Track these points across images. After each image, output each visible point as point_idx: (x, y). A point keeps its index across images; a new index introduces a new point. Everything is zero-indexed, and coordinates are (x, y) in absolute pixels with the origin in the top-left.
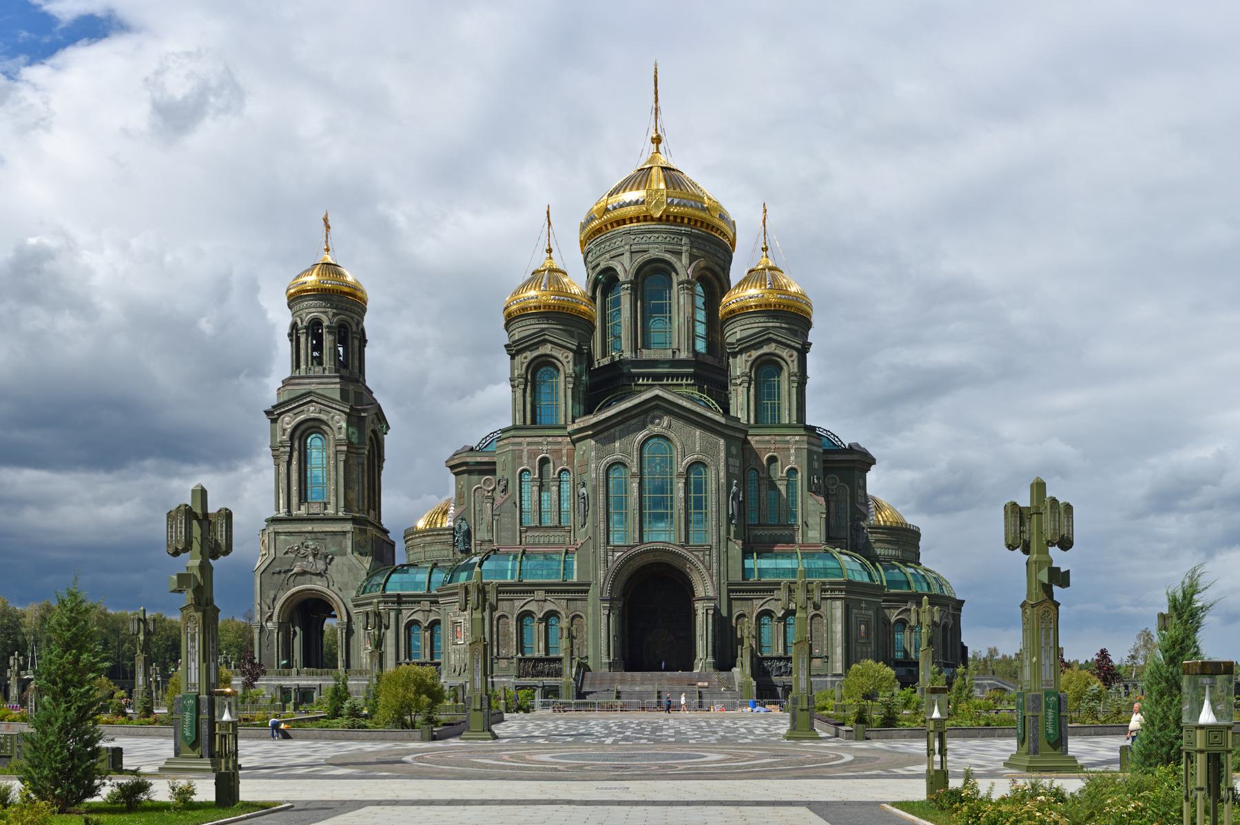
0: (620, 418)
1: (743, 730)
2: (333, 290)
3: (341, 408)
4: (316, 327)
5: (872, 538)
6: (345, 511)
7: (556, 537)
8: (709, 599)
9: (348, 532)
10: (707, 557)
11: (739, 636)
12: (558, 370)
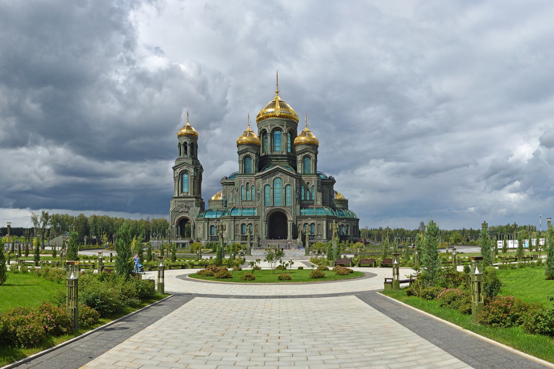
5: (335, 203)
7: (251, 203)
8: (291, 221)
9: (194, 201)
10: (291, 209)
11: (299, 231)
12: (251, 158)
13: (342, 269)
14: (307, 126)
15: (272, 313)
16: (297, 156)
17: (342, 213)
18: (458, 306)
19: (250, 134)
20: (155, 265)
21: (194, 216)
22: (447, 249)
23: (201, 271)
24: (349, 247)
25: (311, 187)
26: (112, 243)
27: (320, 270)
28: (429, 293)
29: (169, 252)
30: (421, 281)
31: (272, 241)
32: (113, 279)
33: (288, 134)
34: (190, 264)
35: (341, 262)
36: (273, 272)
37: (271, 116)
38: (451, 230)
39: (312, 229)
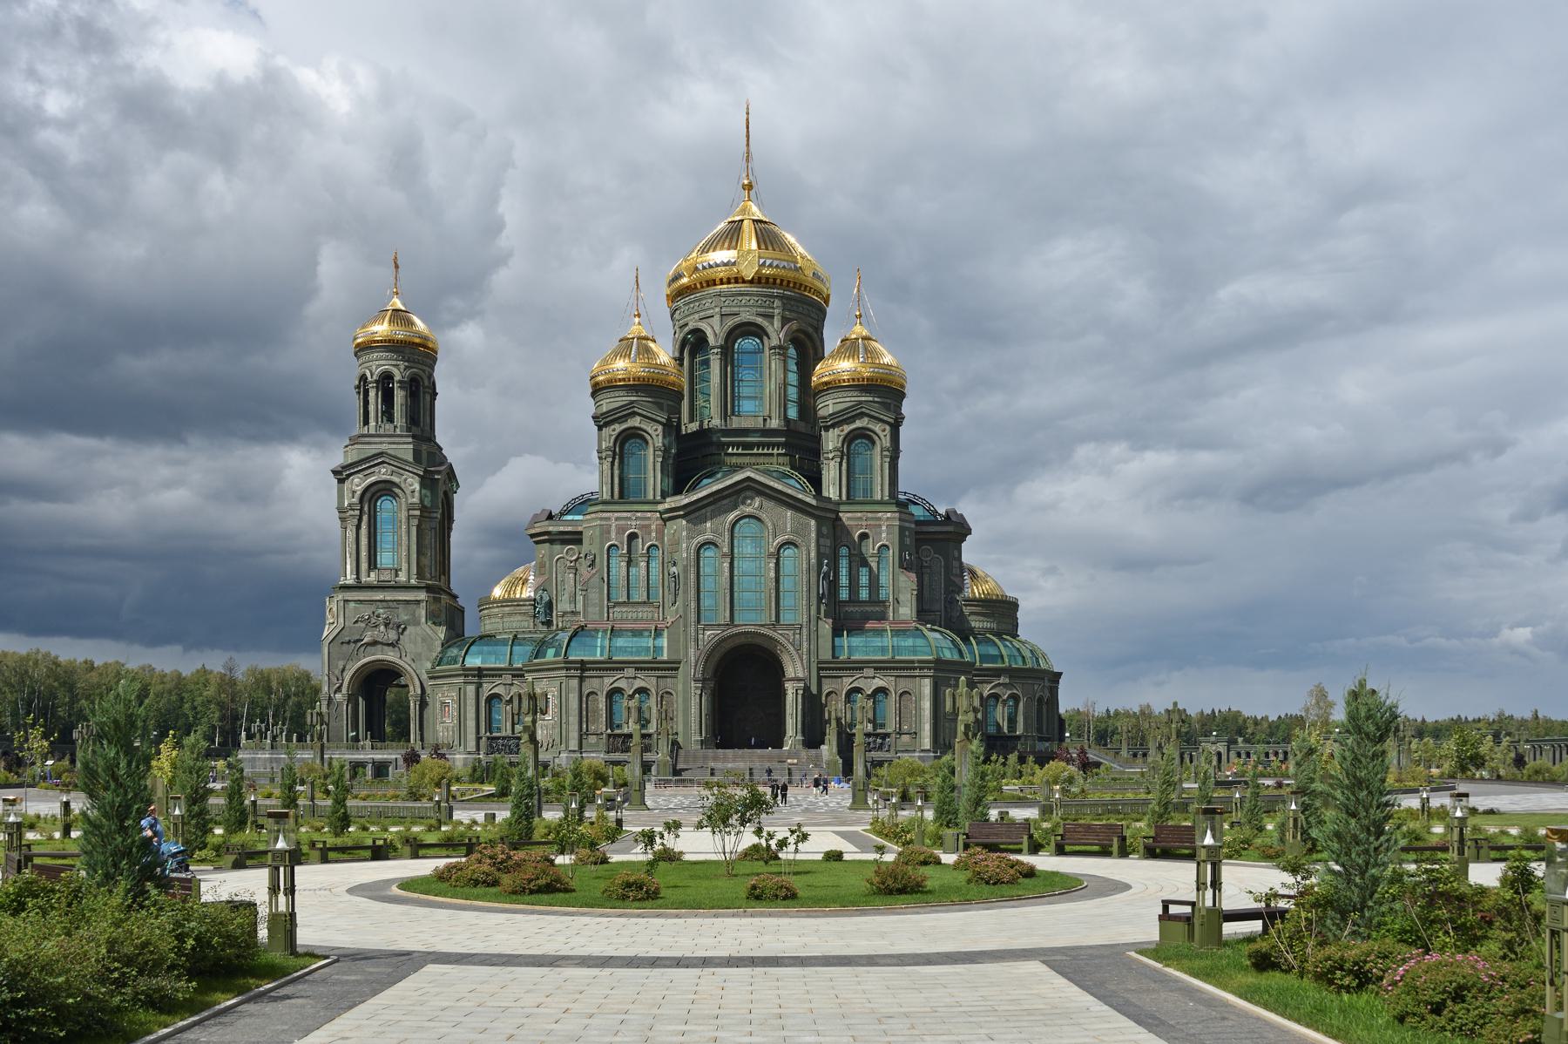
0: (712, 499)
1: (821, 804)
2: (406, 341)
3: (415, 471)
4: (386, 381)
5: (966, 610)
6: (417, 578)
7: (644, 613)
8: (799, 680)
10: (797, 636)
12: (647, 443)
13: (991, 861)
14: (861, 316)
15: (724, 1021)
16: (823, 433)
17: (992, 651)
18: (1476, 1024)
19: (642, 346)
20: (261, 847)
21: (421, 660)
22: (1425, 796)
23: (449, 868)
24: (1020, 777)
25: (875, 552)
26: (73, 761)
27: (906, 864)
28: (1347, 966)
29: (318, 795)
30: (1313, 915)
31: (724, 754)
32: (69, 905)
33: (787, 349)
34: (407, 841)
35: (988, 836)
36: (728, 868)
37: (725, 280)
38: (1440, 719)
39: (878, 712)
